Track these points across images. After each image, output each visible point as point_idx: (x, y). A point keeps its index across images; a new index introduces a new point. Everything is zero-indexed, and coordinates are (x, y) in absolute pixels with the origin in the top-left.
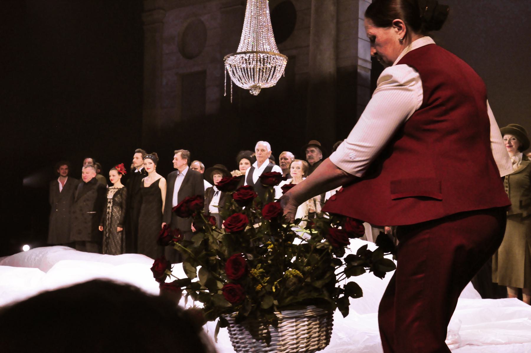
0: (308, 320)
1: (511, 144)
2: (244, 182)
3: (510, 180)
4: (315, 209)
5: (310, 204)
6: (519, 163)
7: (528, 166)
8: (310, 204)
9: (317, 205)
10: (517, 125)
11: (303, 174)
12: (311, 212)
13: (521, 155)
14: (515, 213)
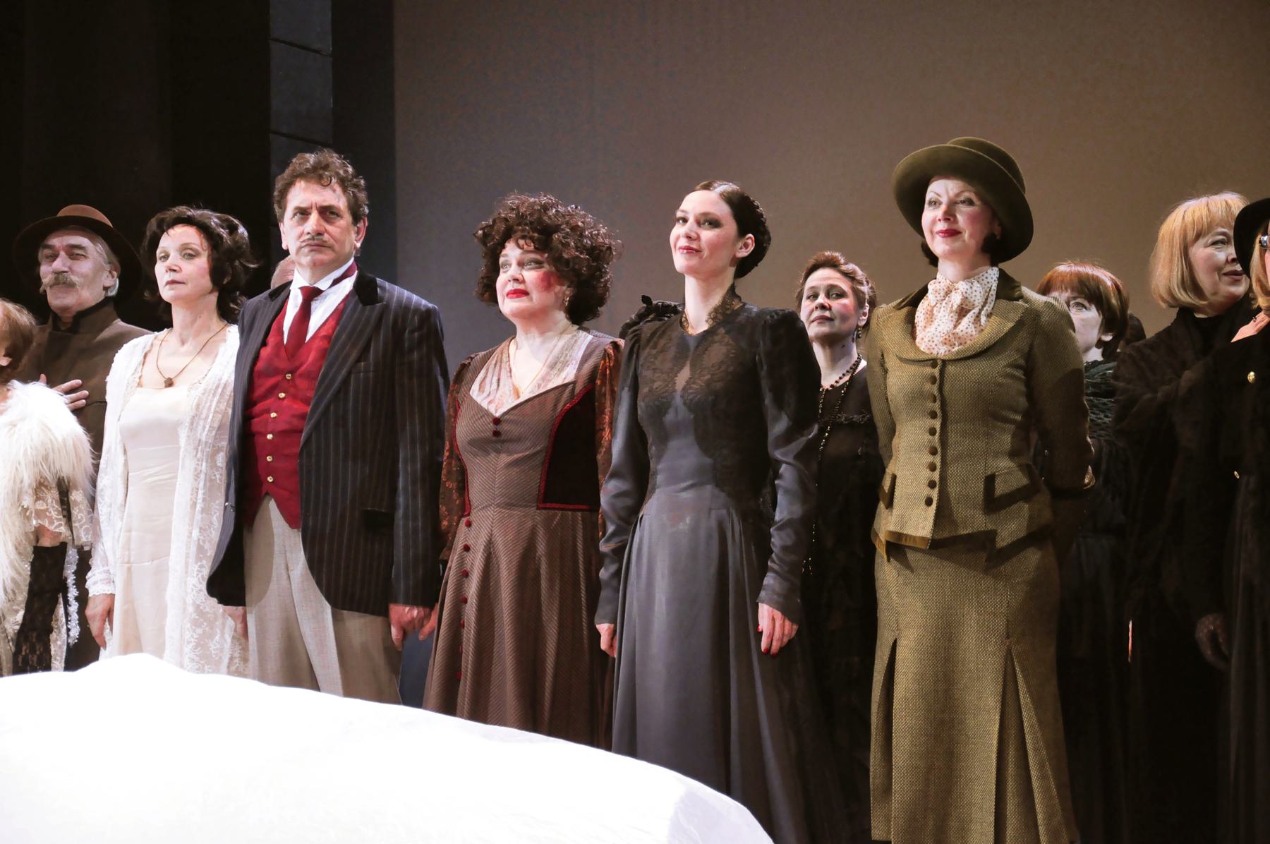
1: (956, 221)
3: (947, 388)
4: (63, 529)
5: (41, 506)
6: (983, 313)
7: (1020, 324)
8: (41, 506)
10: (973, 150)
12: (46, 542)
13: (992, 274)
14: (963, 532)
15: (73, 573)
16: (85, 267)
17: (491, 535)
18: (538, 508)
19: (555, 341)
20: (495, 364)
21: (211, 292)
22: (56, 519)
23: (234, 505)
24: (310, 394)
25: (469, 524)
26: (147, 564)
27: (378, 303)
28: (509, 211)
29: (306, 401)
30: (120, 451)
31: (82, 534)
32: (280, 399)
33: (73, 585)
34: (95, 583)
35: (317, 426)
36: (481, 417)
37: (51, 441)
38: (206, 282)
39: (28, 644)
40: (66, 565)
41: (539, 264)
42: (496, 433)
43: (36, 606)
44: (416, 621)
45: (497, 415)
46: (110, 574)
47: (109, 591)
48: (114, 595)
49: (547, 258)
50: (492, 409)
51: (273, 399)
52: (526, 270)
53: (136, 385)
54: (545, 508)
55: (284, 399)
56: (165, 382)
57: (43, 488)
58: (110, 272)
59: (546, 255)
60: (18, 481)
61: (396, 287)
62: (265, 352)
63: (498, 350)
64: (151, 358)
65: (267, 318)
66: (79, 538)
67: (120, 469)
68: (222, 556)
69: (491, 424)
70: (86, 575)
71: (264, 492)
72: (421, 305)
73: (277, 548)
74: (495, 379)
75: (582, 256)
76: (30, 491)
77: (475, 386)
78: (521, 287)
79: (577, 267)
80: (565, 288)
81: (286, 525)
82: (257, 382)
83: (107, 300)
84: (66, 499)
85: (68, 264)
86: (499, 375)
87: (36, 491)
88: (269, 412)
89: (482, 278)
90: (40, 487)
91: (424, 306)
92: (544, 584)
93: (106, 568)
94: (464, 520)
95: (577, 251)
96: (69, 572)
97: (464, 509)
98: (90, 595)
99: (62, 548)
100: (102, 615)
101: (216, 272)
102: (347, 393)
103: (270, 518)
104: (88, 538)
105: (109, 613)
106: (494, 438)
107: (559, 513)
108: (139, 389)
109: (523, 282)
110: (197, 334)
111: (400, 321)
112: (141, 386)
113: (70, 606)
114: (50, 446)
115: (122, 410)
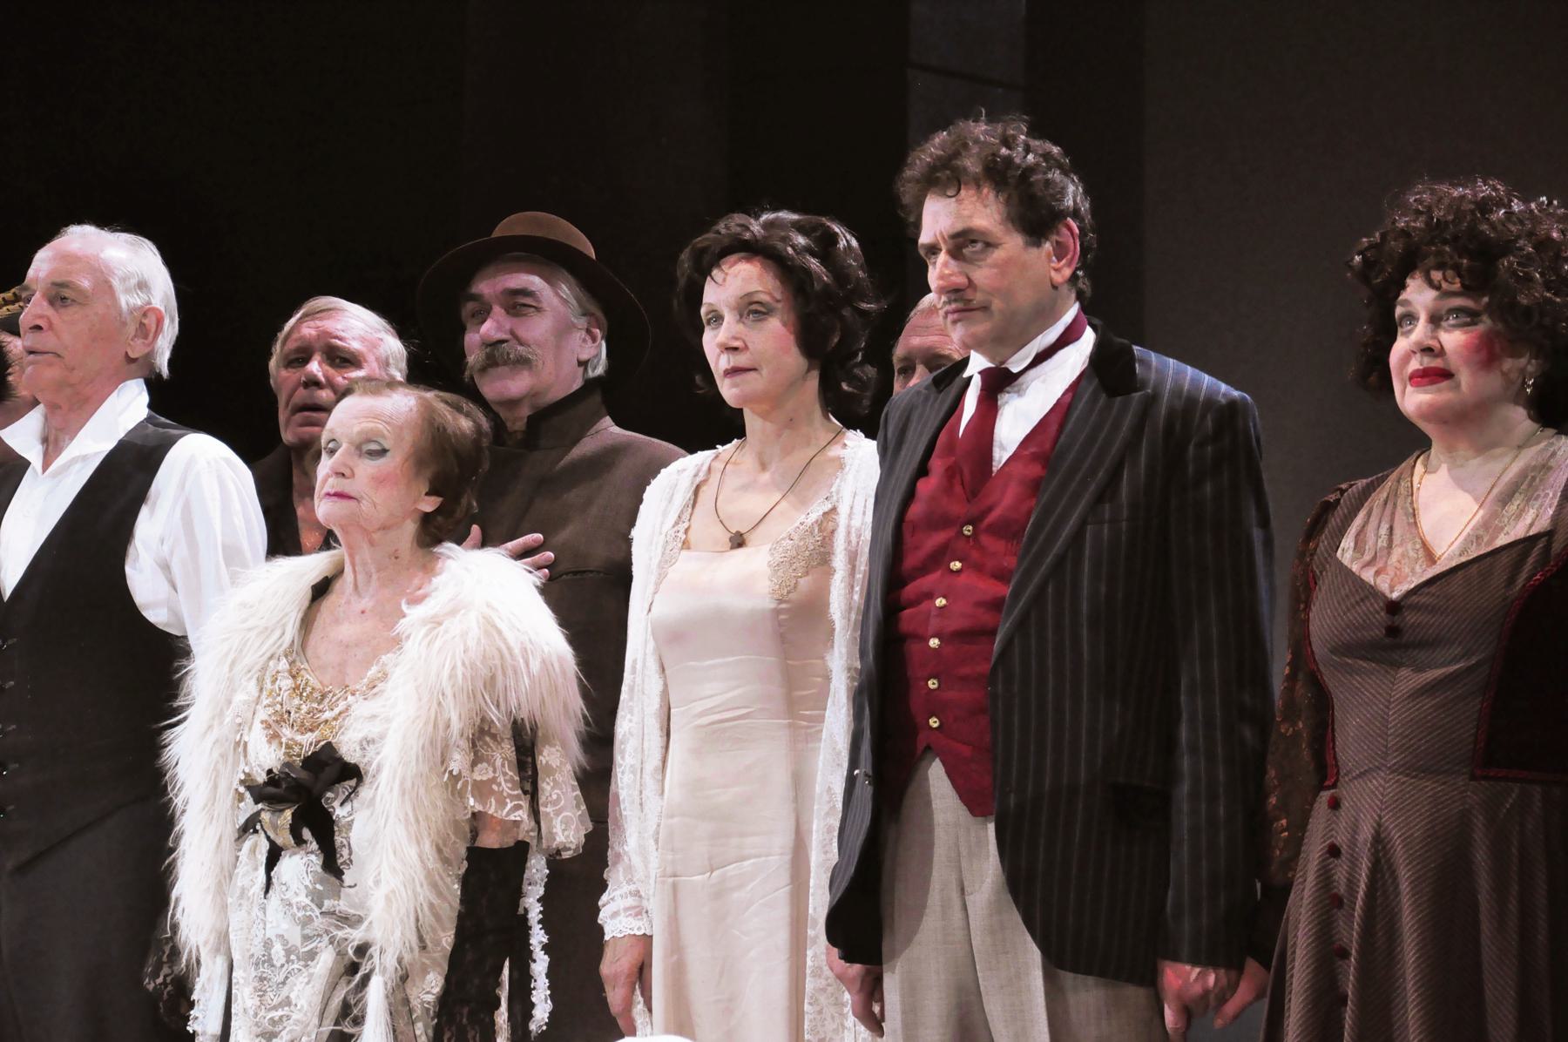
0: (954, 162)
2: (967, 426)
4: (522, 815)
5: (482, 773)
8: (482, 773)
9: (546, 787)
11: (429, 505)
12: (490, 840)
15: (539, 901)
16: (538, 329)
17: (1379, 825)
18: (1473, 778)
19: (1507, 459)
20: (1386, 503)
21: (808, 371)
22: (510, 796)
23: (870, 773)
24: (1009, 562)
25: (1335, 804)
26: (699, 878)
27: (1136, 391)
28: (1413, 217)
29: (1002, 576)
30: (653, 666)
31: (558, 828)
32: (952, 571)
33: (539, 922)
34: (615, 914)
35: (1022, 625)
36: (1362, 600)
37: (500, 651)
38: (794, 360)
39: (454, 1028)
40: (526, 888)
41: (1470, 317)
42: (1393, 631)
43: (469, 957)
44: (1212, 997)
45: (1395, 595)
46: (640, 897)
47: (639, 929)
48: (651, 937)
49: (1488, 305)
50: (1383, 585)
51: (939, 573)
52: (1446, 331)
53: (680, 545)
54: (1485, 778)
55: (959, 571)
56: (731, 540)
57: (488, 739)
58: (588, 331)
59: (1486, 299)
60: (441, 726)
61: (1171, 360)
62: (926, 487)
63: (1394, 476)
64: (707, 494)
65: (929, 425)
66: (552, 836)
67: (653, 704)
68: (852, 869)
69: (1382, 614)
70: (599, 898)
71: (921, 746)
72: (1218, 392)
73: (940, 852)
74: (1384, 531)
75: (1558, 300)
76: (464, 744)
77: (1347, 543)
78: (1437, 363)
79: (1547, 321)
80: (1523, 361)
81: (962, 811)
82: (908, 540)
83: (590, 385)
84: (530, 760)
85: (508, 327)
86: (1392, 520)
87: (474, 745)
88: (931, 596)
89: (1366, 345)
90: (481, 735)
91: (1224, 395)
92: (1486, 927)
93: (632, 887)
94: (1325, 795)
95: (1549, 290)
96: (531, 900)
97: (1325, 771)
98: (607, 938)
99: (520, 852)
100: (629, 976)
101: (810, 339)
102: (1078, 563)
103: (928, 794)
104: (568, 837)
105: (641, 973)
106: (1387, 641)
107: (1516, 789)
108: (684, 553)
109: (1441, 353)
110: (787, 451)
111: (1178, 427)
112: (689, 548)
113: (535, 961)
114: (498, 662)
115: (655, 593)
